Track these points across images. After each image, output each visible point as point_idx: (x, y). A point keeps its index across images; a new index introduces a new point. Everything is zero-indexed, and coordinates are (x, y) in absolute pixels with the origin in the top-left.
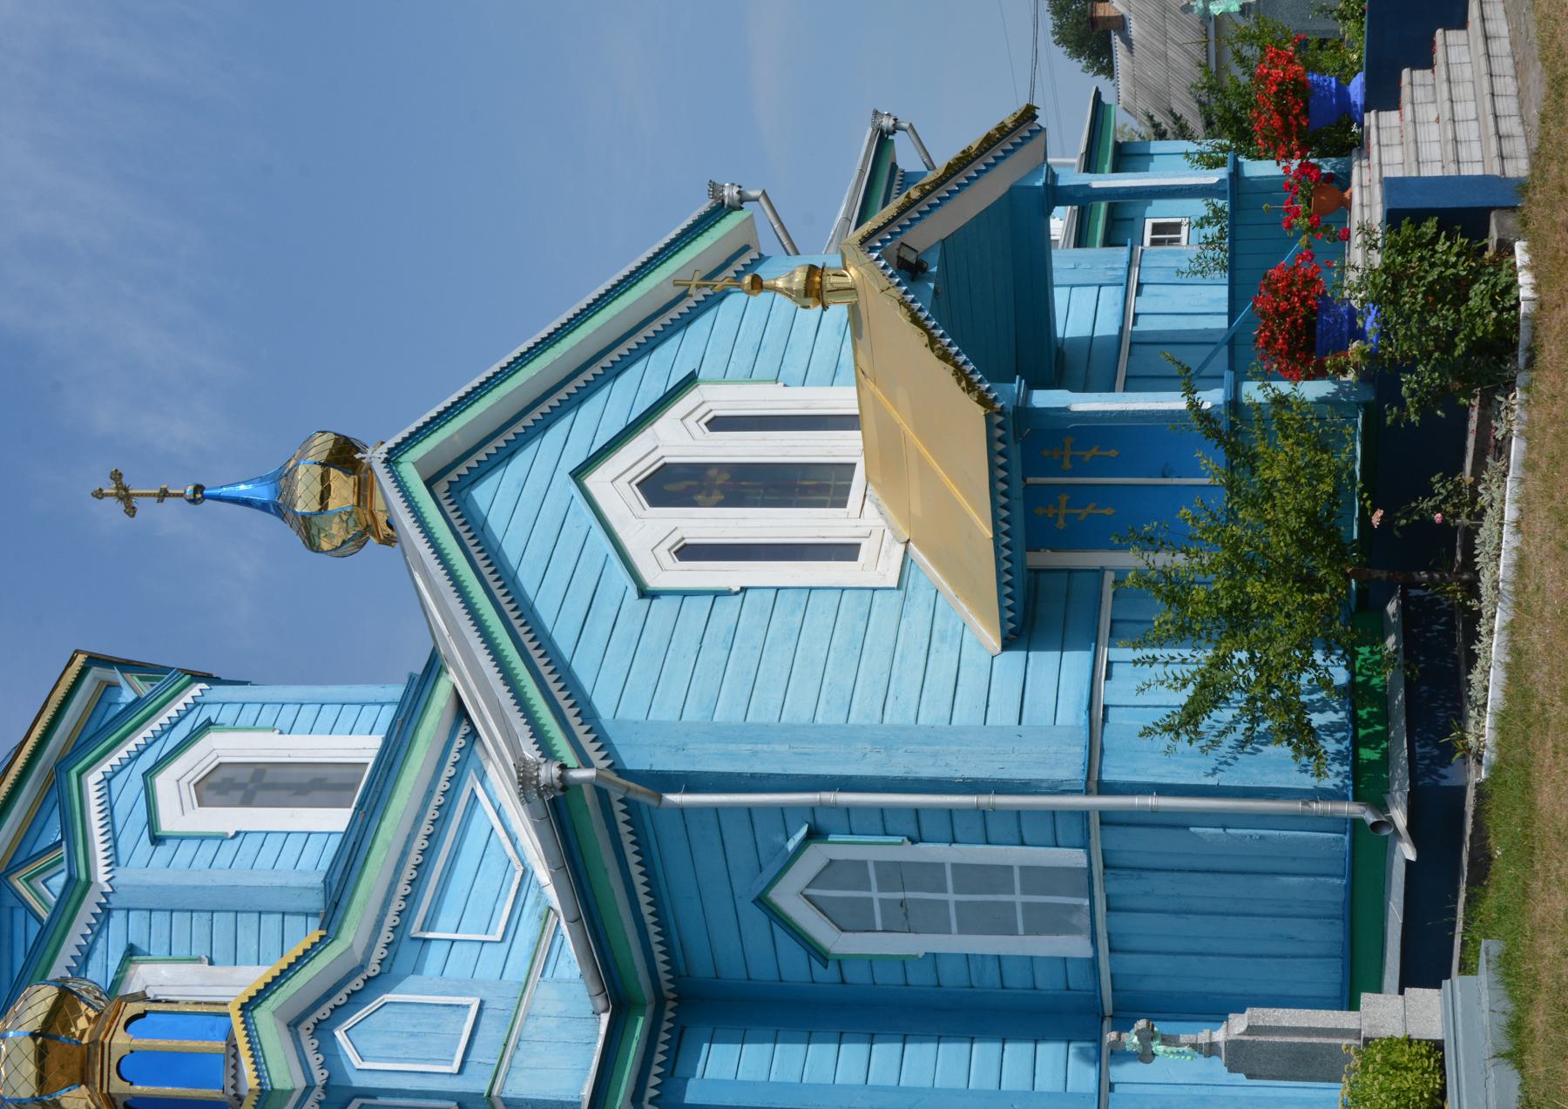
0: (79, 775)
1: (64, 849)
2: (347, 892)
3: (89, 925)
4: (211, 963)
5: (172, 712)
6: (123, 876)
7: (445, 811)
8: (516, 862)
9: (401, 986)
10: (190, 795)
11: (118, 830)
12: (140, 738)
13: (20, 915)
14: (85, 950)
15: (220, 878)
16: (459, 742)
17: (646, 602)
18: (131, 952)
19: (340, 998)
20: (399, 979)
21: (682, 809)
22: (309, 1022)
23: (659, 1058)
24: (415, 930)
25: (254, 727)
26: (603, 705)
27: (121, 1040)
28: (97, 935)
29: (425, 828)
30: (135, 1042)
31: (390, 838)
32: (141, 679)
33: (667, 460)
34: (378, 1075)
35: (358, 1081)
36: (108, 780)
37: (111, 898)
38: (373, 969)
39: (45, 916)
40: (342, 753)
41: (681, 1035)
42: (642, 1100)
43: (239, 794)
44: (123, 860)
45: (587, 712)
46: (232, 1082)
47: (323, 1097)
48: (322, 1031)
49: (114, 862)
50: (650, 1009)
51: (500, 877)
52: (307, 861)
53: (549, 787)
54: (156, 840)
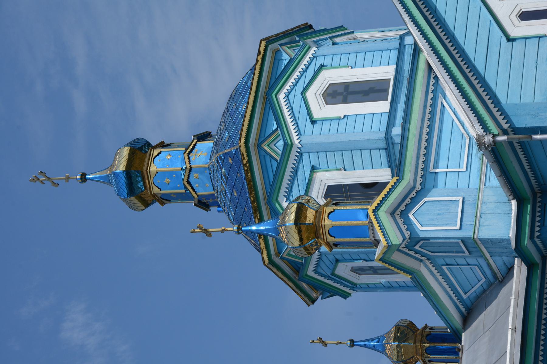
0: (276, 95)
1: (279, 131)
2: (403, 159)
3: (295, 160)
4: (345, 170)
5: (305, 62)
6: (306, 140)
7: (433, 113)
8: (465, 135)
9: (430, 194)
10: (321, 100)
11: (297, 119)
12: (295, 76)
13: (268, 158)
14: (295, 169)
15: (343, 138)
16: (432, 81)
17: (511, 43)
18: (313, 169)
19: (408, 201)
20: (429, 191)
21: (541, 141)
22: (398, 212)
23: (538, 219)
24: (431, 169)
25: (339, 66)
26: (501, 96)
27: (327, 222)
28: (299, 163)
29: (426, 123)
30: (334, 223)
31: (415, 132)
32: (289, 48)
33: (523, 10)
34: (429, 232)
35: (422, 235)
36: (287, 96)
37: (302, 149)
38: (418, 188)
39: (278, 159)
40: (379, 75)
41: (545, 207)
42: (534, 237)
43: (341, 98)
44: (302, 132)
45: (496, 102)
46: (373, 235)
47: (409, 241)
48: (404, 214)
49: (299, 134)
50: (531, 201)
51: (460, 142)
52: (375, 127)
53: (490, 145)
54: (313, 122)
